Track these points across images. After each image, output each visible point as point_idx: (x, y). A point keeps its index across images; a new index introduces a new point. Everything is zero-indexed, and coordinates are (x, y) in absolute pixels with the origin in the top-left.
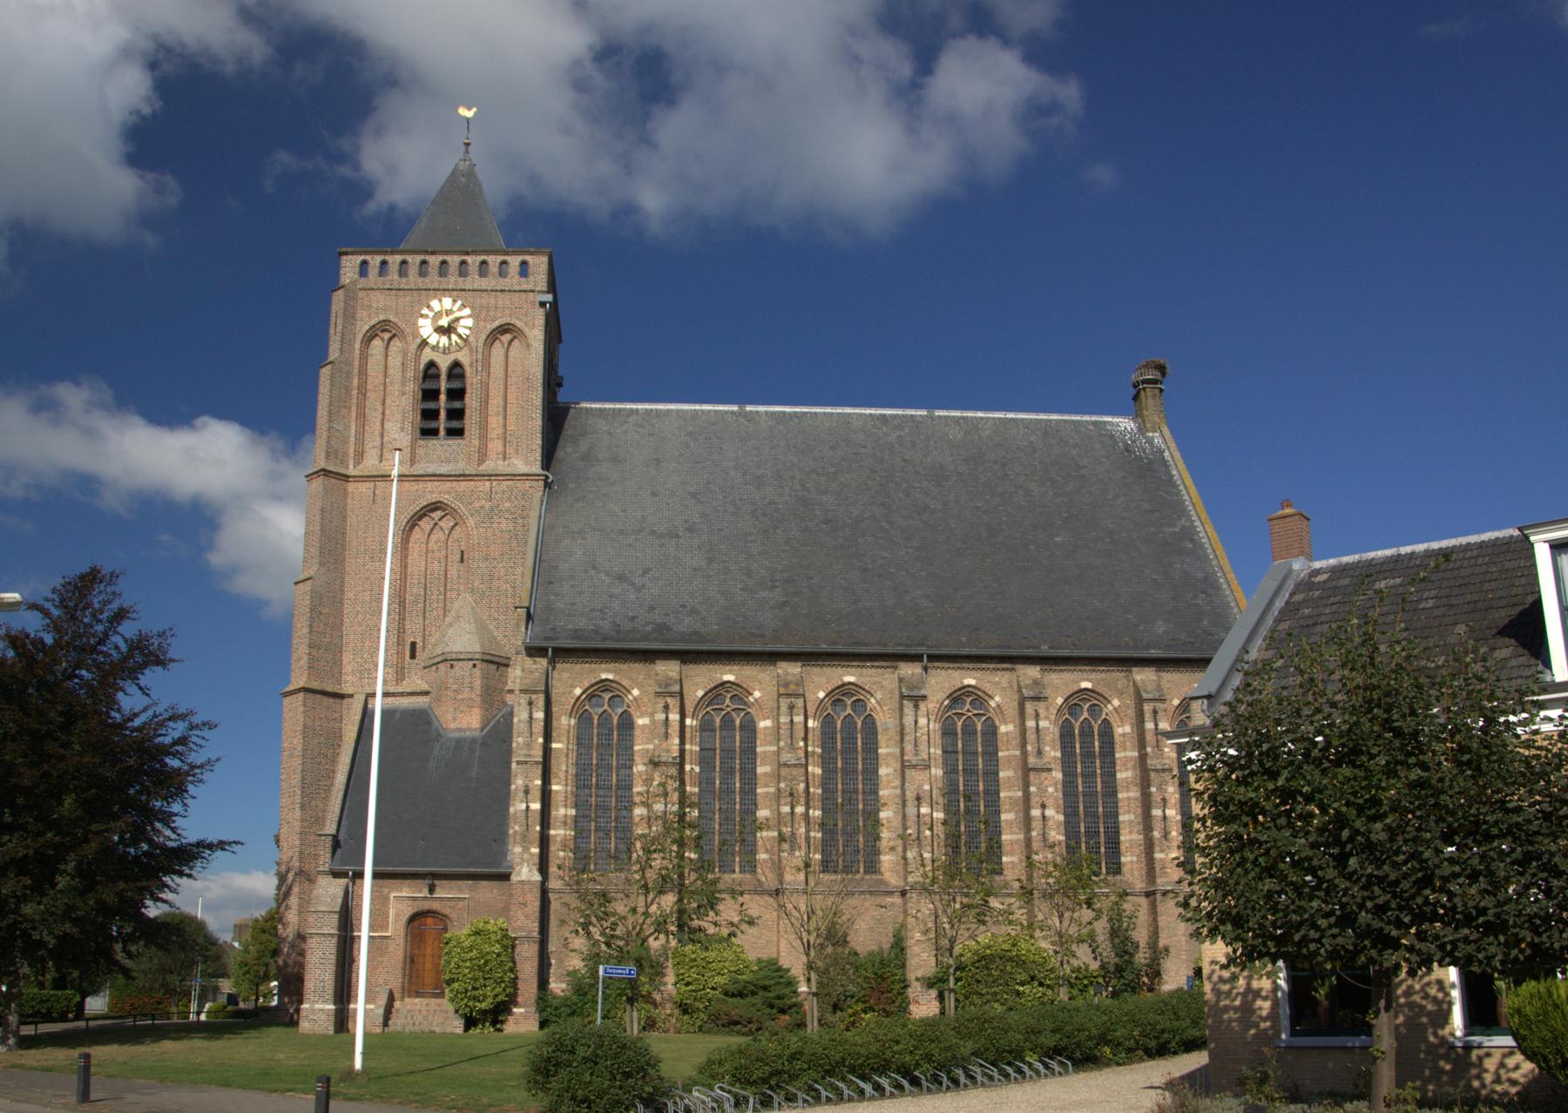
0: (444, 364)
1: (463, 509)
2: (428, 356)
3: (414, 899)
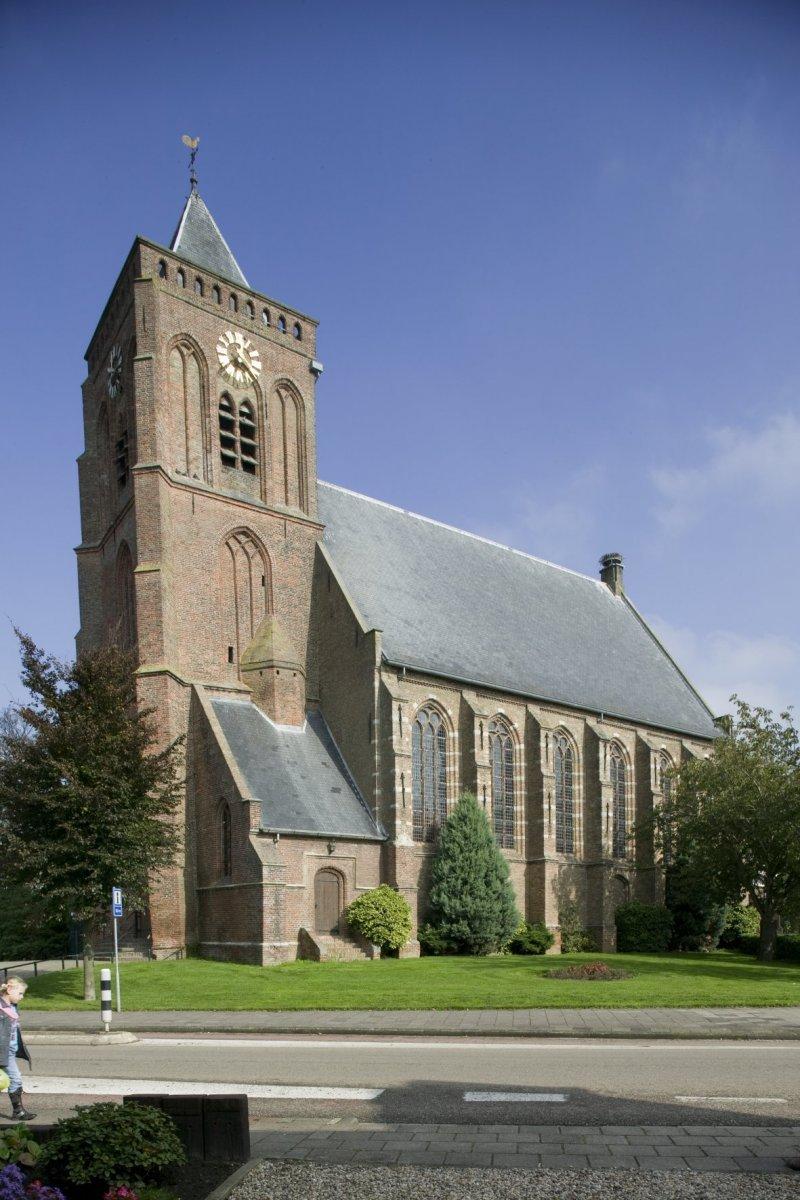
0: (237, 398)
1: (264, 540)
2: (221, 386)
3: (320, 857)
